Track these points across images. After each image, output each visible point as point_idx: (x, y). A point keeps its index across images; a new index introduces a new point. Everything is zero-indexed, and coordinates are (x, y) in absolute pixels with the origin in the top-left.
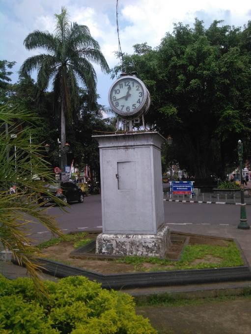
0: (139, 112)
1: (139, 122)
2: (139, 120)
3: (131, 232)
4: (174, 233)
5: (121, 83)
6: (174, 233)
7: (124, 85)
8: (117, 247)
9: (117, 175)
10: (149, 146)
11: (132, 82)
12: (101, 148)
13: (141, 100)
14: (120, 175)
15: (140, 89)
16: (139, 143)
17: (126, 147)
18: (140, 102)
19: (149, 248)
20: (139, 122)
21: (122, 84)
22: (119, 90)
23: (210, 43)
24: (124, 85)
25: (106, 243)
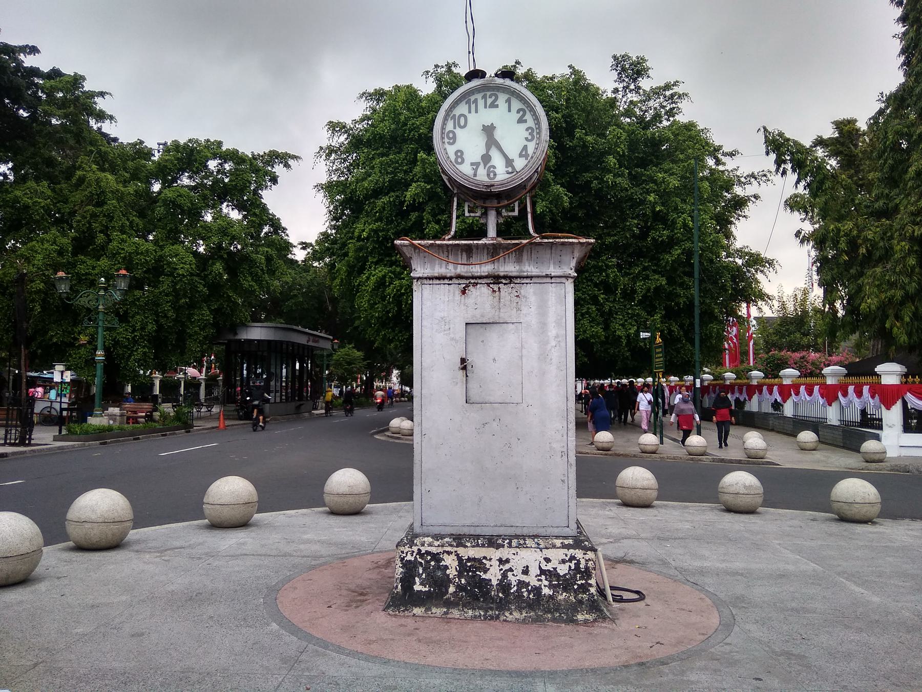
0: (522, 186)
1: (516, 213)
2: (517, 209)
3: (502, 531)
4: (631, 562)
5: (472, 98)
6: (631, 562)
7: (481, 103)
8: (460, 575)
9: (463, 361)
10: (563, 280)
11: (506, 96)
12: (418, 278)
13: (530, 151)
14: (470, 359)
15: (528, 116)
16: (530, 269)
17: (496, 279)
18: (526, 156)
19: (558, 576)
20: (516, 213)
21: (476, 101)
22: (465, 117)
23: (626, 290)
24: (481, 103)
25: (428, 562)
